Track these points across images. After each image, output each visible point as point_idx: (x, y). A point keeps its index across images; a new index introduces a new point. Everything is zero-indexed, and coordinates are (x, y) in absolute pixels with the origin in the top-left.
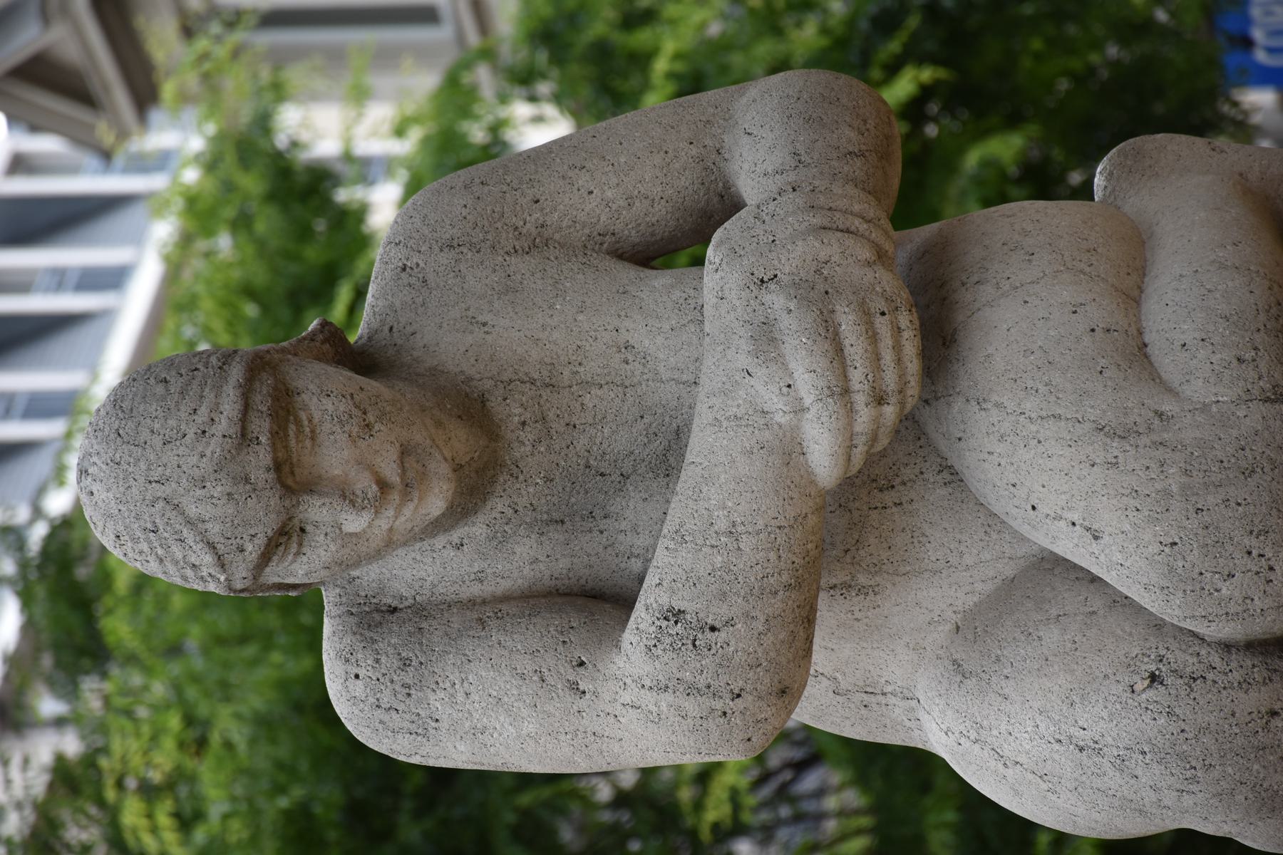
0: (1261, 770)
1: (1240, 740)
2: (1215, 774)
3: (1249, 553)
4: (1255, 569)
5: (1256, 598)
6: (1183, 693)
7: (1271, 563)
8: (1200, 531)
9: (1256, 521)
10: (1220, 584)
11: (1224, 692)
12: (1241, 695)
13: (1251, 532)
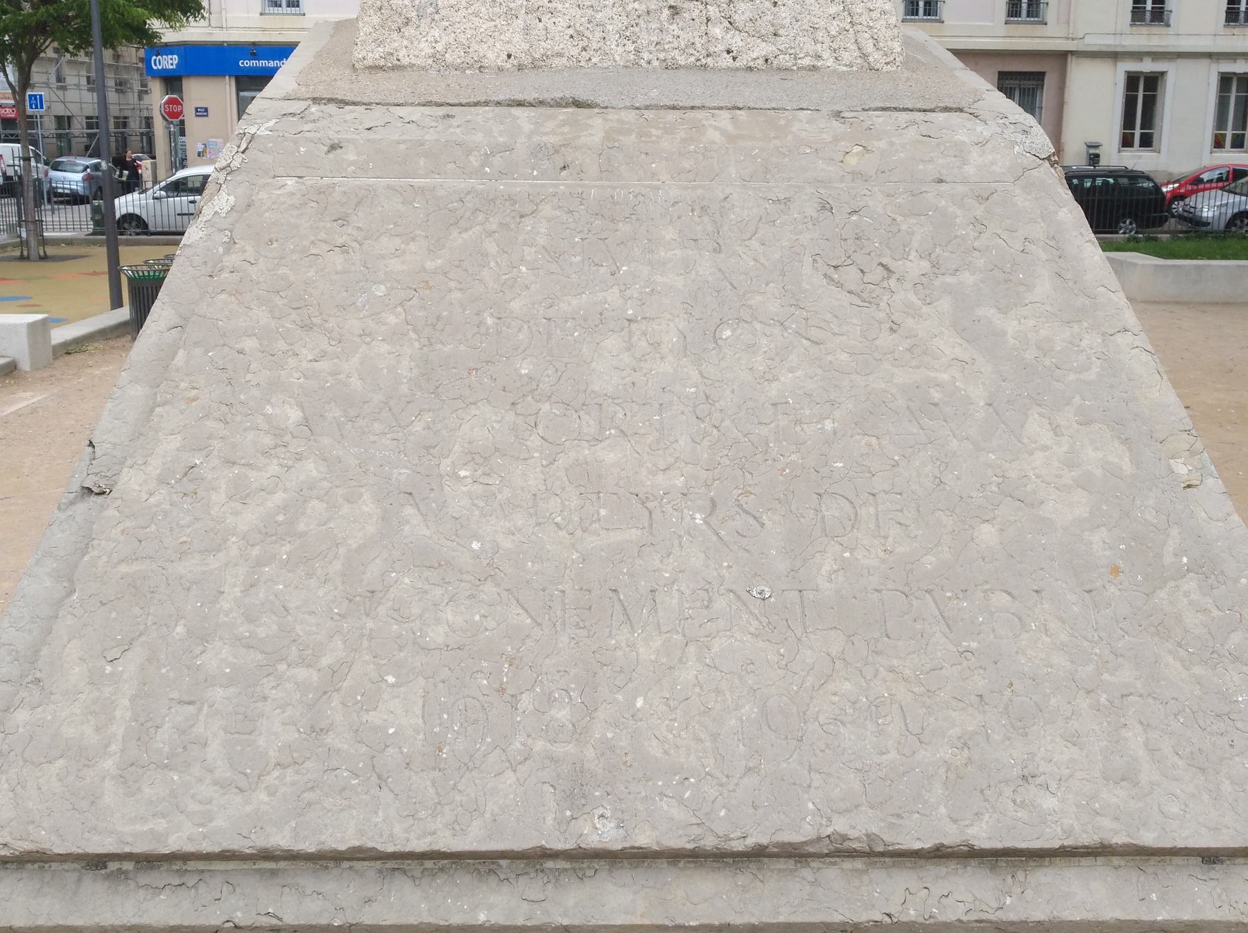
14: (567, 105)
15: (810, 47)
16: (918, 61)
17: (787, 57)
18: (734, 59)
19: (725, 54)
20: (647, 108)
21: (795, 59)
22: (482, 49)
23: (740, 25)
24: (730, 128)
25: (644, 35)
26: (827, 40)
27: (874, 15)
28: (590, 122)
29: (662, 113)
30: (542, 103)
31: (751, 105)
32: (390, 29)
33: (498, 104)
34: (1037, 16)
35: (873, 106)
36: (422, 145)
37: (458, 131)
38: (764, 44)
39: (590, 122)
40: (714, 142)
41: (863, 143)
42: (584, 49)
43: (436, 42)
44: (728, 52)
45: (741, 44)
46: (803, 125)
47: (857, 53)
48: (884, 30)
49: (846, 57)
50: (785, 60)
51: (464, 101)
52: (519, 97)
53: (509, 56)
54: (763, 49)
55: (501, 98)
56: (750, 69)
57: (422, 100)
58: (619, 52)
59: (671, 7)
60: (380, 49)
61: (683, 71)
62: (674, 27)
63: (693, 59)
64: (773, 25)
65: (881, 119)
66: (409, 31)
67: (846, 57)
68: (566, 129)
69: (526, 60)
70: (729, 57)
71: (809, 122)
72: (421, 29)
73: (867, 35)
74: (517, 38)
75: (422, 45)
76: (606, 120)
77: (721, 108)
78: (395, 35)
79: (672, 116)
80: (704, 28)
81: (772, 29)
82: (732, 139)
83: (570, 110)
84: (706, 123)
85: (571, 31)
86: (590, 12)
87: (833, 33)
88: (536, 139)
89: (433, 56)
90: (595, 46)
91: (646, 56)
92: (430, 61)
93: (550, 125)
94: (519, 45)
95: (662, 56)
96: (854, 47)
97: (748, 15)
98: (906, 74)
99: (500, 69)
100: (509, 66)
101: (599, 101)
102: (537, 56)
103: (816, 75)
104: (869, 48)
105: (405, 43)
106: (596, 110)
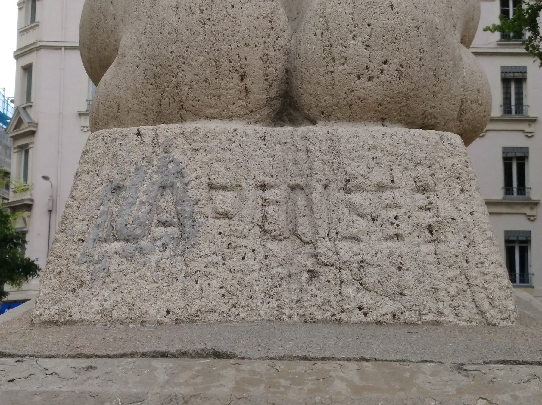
0: (198, 63)
1: (225, 48)
2: (197, 27)
3: (385, 63)
4: (372, 66)
5: (344, 67)
6: (261, 11)
7: (375, 79)
8: (404, 27)
9: (408, 70)
10: (359, 39)
11: (262, 41)
12: (260, 54)
13: (401, 66)
14: (208, 356)
15: (432, 304)
16: (529, 317)
17: (412, 313)
18: (365, 314)
19: (357, 311)
20: (281, 358)
21: (420, 314)
22: (145, 306)
23: (370, 286)
24: (356, 379)
25: (286, 294)
26: (447, 299)
27: (489, 278)
28: (223, 372)
29: (293, 363)
30: (184, 354)
31: (378, 357)
32: (66, 290)
33: (144, 355)
34: (528, 283)
35: (494, 359)
36: (57, 396)
37: (95, 382)
38: (391, 302)
39: (223, 372)
40: (340, 394)
41: (486, 396)
42: (234, 306)
43: (106, 300)
44: (360, 308)
45: (370, 302)
46: (426, 377)
47: (475, 311)
48: (497, 290)
49: (465, 314)
50: (411, 316)
51: (111, 353)
52: (163, 348)
53: (168, 312)
54: (390, 306)
55: (147, 349)
56: (379, 323)
57: (73, 352)
58: (264, 309)
59: (309, 271)
60: (56, 307)
61: (320, 325)
62: (312, 287)
63: (328, 314)
64: (399, 286)
65: (502, 373)
66: (83, 292)
67: (465, 314)
68: (199, 380)
69: (182, 315)
70: (360, 314)
71: (433, 374)
72: (93, 290)
73: (482, 295)
74: (177, 297)
75: (93, 303)
76: (238, 370)
77: (349, 360)
78: (70, 295)
79: (301, 367)
80: (338, 288)
81: (398, 290)
82: (357, 390)
83: (207, 361)
84: (332, 373)
85: (223, 291)
86: (240, 275)
87: (453, 293)
88: (168, 390)
89: (102, 312)
90: (243, 303)
91: (287, 311)
92: (98, 317)
93: (185, 376)
94: (177, 303)
95: (301, 312)
96: (472, 305)
97: (376, 278)
98: (522, 329)
99: (160, 323)
100: (167, 320)
101: (237, 352)
102: (192, 312)
103: (439, 329)
104: (485, 305)
105: (78, 301)
106: (232, 361)
